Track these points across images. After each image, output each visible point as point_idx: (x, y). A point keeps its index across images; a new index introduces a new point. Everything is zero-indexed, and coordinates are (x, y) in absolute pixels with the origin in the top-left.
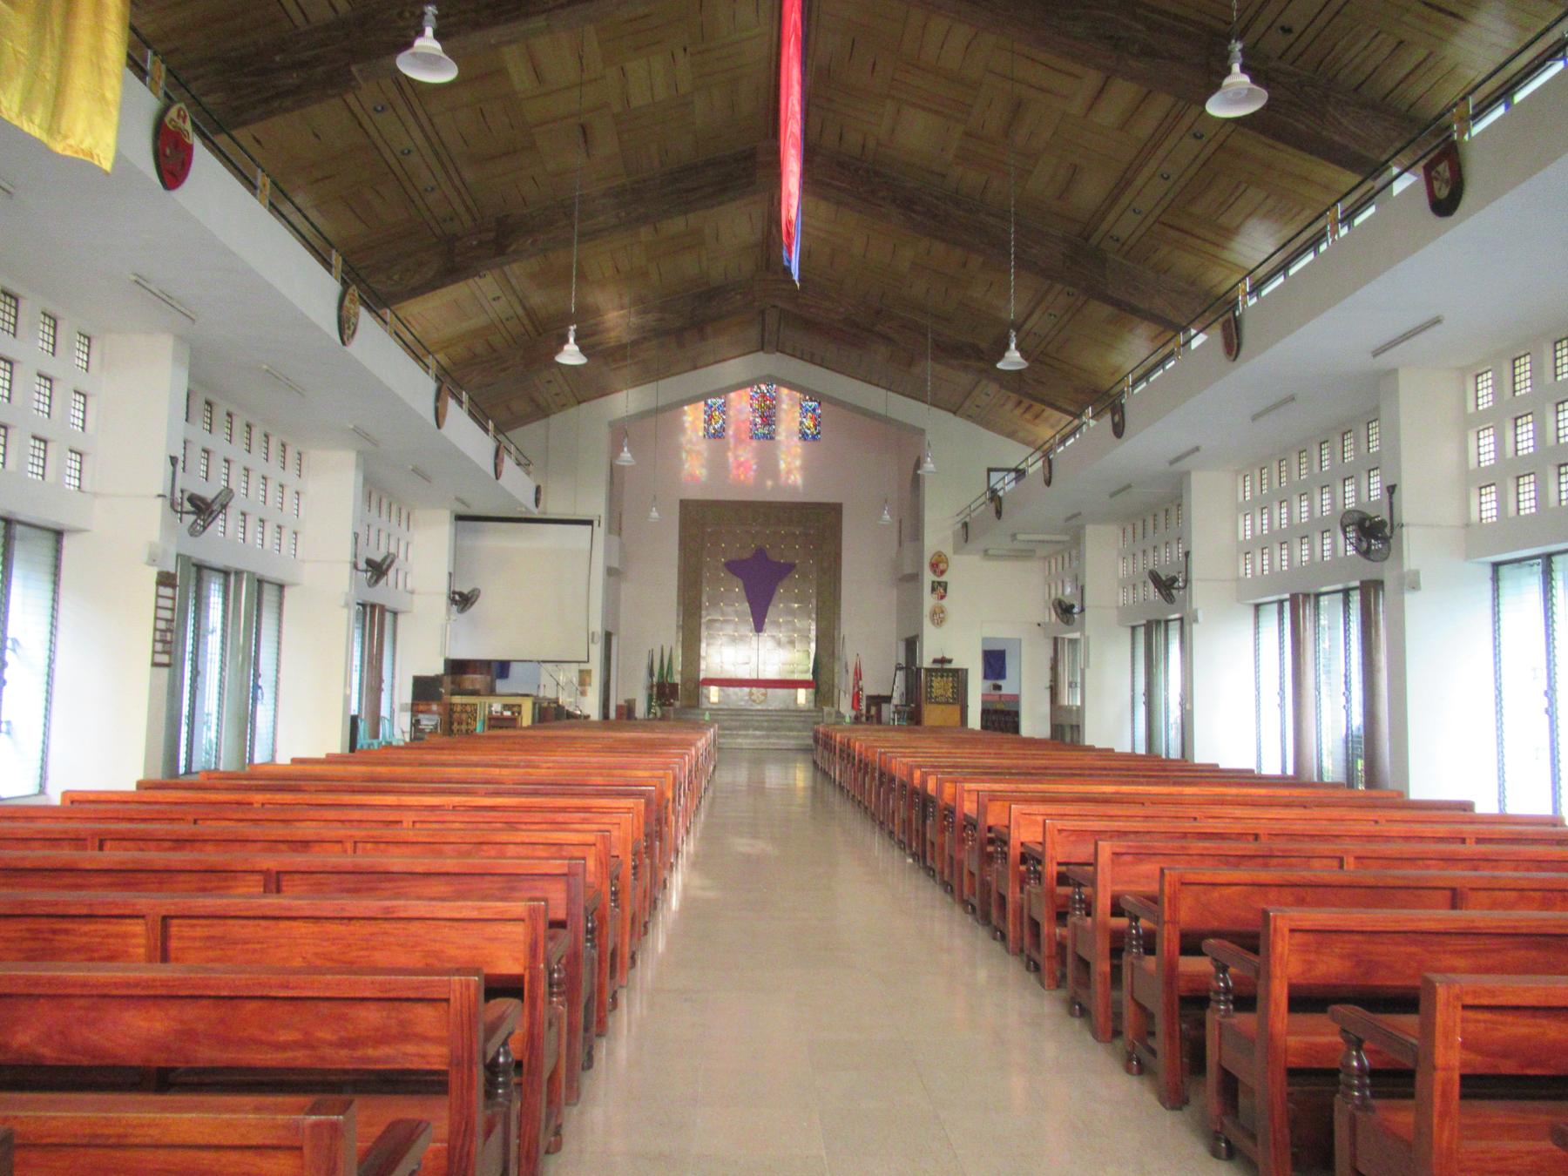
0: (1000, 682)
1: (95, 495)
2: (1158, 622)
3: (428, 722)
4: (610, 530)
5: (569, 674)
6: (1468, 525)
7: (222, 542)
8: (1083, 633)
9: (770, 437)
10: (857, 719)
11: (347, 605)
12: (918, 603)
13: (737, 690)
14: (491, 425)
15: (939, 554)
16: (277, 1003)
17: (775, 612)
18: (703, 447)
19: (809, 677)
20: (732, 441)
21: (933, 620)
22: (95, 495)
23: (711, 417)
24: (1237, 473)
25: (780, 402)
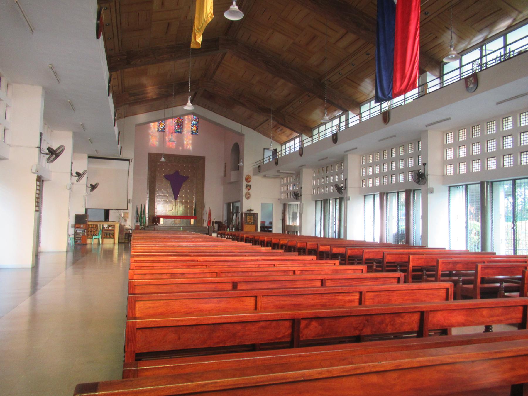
1: (10, 146)
2: (327, 200)
6: (443, 175)
8: (301, 202)
9: (181, 132)
15: (248, 175)
16: (154, 329)
17: (182, 193)
18: (157, 134)
20: (167, 133)
22: (10, 146)
24: (360, 156)
25: (185, 121)
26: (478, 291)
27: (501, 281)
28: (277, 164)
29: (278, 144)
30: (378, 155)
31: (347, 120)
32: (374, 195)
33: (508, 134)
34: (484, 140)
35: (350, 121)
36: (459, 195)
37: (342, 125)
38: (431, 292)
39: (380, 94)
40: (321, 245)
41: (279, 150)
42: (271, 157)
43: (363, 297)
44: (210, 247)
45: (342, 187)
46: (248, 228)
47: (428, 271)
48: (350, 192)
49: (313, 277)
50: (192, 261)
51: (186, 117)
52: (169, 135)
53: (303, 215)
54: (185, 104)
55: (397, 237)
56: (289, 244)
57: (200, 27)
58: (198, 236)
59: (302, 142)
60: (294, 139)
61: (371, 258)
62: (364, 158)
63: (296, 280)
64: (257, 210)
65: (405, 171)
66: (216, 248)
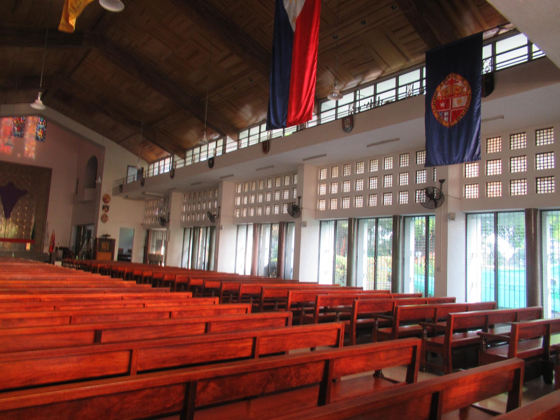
2: (197, 228)
6: (316, 210)
9: (22, 136)
17: (16, 211)
25: (28, 122)
26: (354, 328)
27: (340, 310)
28: (142, 184)
29: (144, 161)
30: (254, 184)
31: (224, 145)
33: (374, 175)
34: (353, 179)
35: (227, 146)
36: (328, 232)
37: (218, 149)
38: (323, 333)
39: (273, 121)
40: (193, 278)
41: (146, 169)
42: (136, 176)
43: (257, 343)
44: (57, 280)
45: (215, 215)
46: (101, 256)
47: (280, 301)
48: (223, 221)
49: (197, 320)
50: (33, 300)
51: (30, 118)
53: (169, 244)
54: (33, 102)
55: (269, 269)
56: (155, 276)
57: (75, 6)
58: (37, 265)
59: (173, 163)
60: (164, 159)
61: (247, 293)
63: (175, 325)
64: (115, 235)
65: (281, 203)
66: (65, 282)
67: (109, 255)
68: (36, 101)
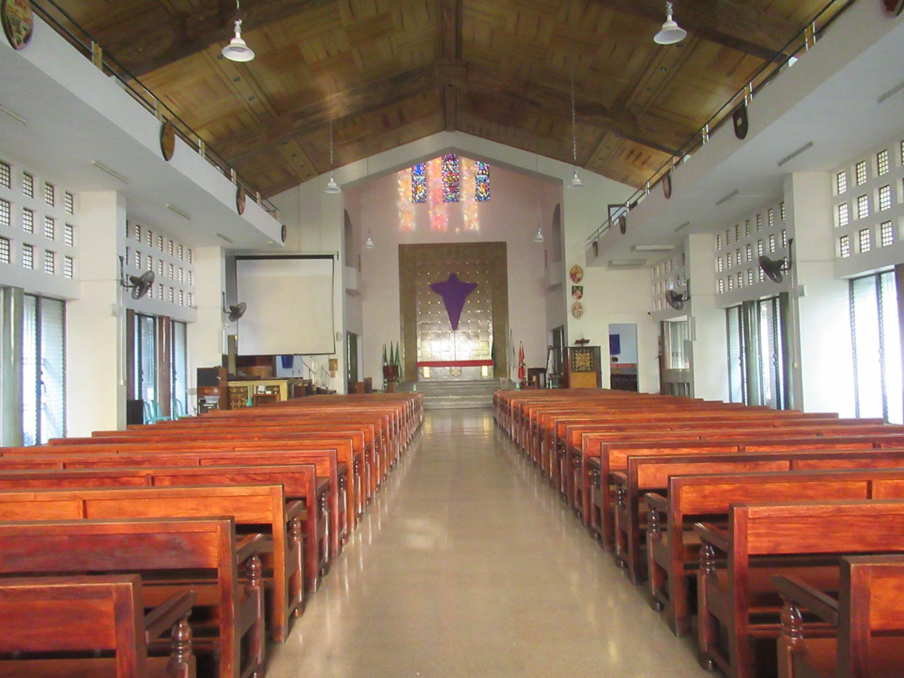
0: (616, 356)
2: (752, 303)
3: (211, 401)
4: (348, 263)
5: (325, 360)
7: (153, 301)
8: (689, 315)
9: (456, 200)
10: (523, 386)
11: (114, 314)
12: (563, 300)
13: (441, 368)
14: (258, 195)
15: (576, 267)
19: (489, 358)
20: (431, 203)
21: (573, 314)
23: (416, 189)
25: (462, 176)
32: (879, 275)
52: (434, 207)
62: (843, 178)
67: (592, 377)
68: (233, 41)
